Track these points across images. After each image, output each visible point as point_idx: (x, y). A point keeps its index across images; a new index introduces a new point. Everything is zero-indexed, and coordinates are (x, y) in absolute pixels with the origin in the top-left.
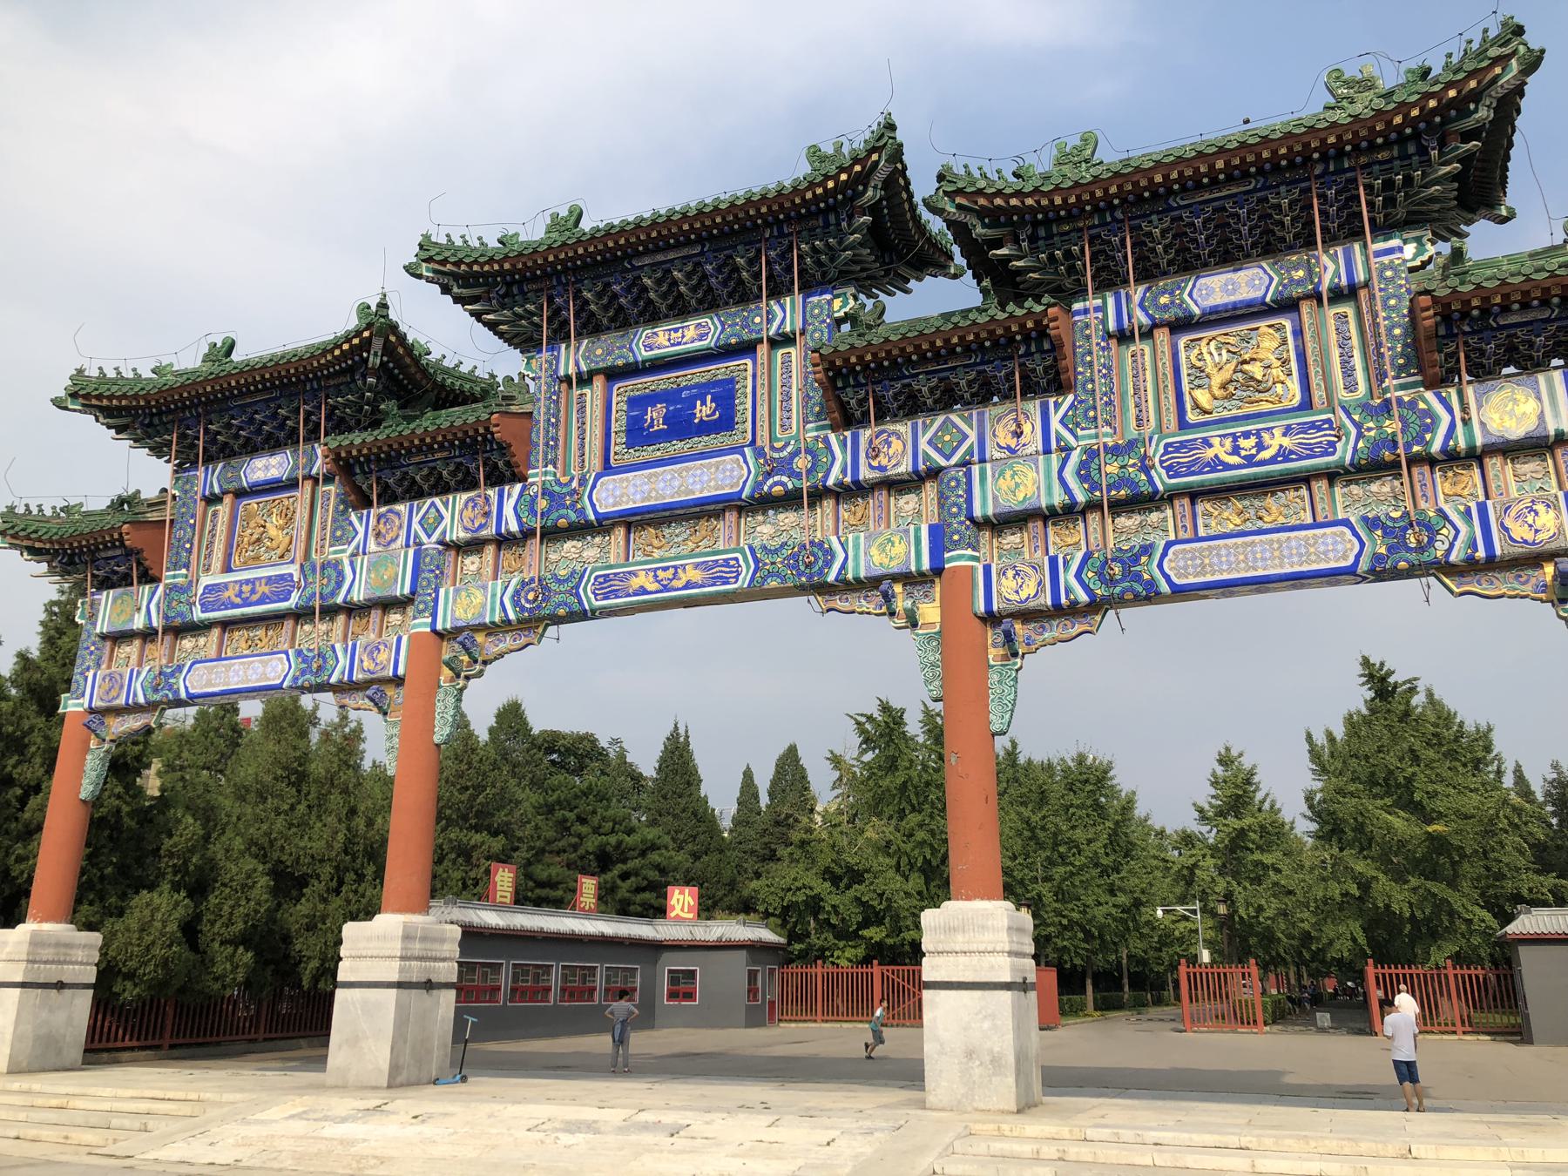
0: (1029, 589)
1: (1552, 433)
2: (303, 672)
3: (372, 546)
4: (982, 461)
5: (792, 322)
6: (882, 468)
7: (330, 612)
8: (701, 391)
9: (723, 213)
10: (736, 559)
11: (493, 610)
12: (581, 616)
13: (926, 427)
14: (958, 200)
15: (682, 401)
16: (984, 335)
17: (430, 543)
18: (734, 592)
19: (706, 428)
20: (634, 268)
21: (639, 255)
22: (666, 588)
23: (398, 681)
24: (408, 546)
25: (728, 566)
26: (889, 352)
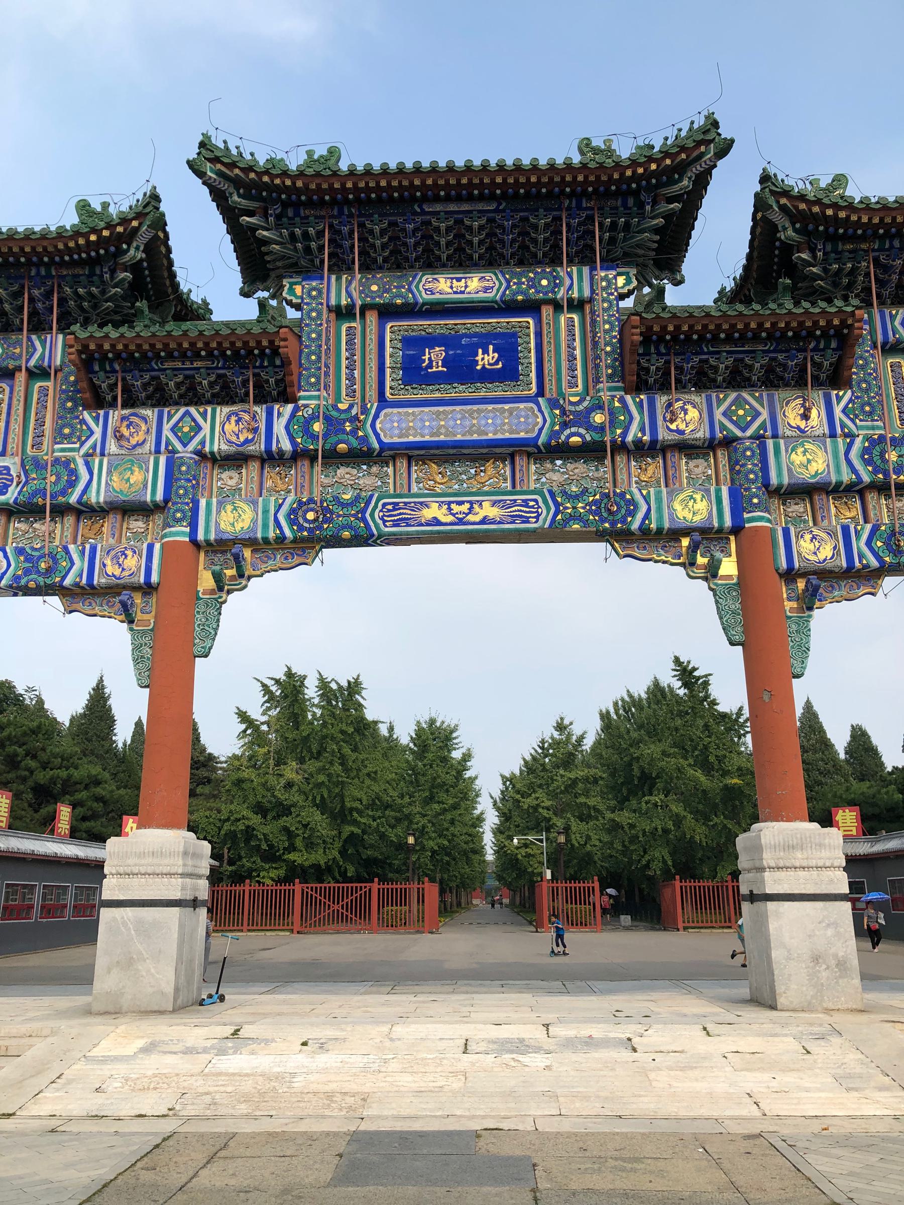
0: (826, 552)
1: (834, 481)
2: (27, 572)
3: (112, 447)
4: (775, 436)
5: (580, 290)
6: (681, 432)
7: (60, 511)
8: (483, 340)
9: (493, 174)
10: (536, 501)
11: (265, 526)
12: (363, 539)
13: (720, 402)
14: (783, 201)
15: (461, 347)
16: (226, 345)
17: (186, 452)
18: (534, 531)
19: (487, 376)
20: (423, 213)
21: (437, 199)
22: (461, 522)
23: (148, 589)
24: (158, 451)
25: (527, 506)
26: (139, 346)
